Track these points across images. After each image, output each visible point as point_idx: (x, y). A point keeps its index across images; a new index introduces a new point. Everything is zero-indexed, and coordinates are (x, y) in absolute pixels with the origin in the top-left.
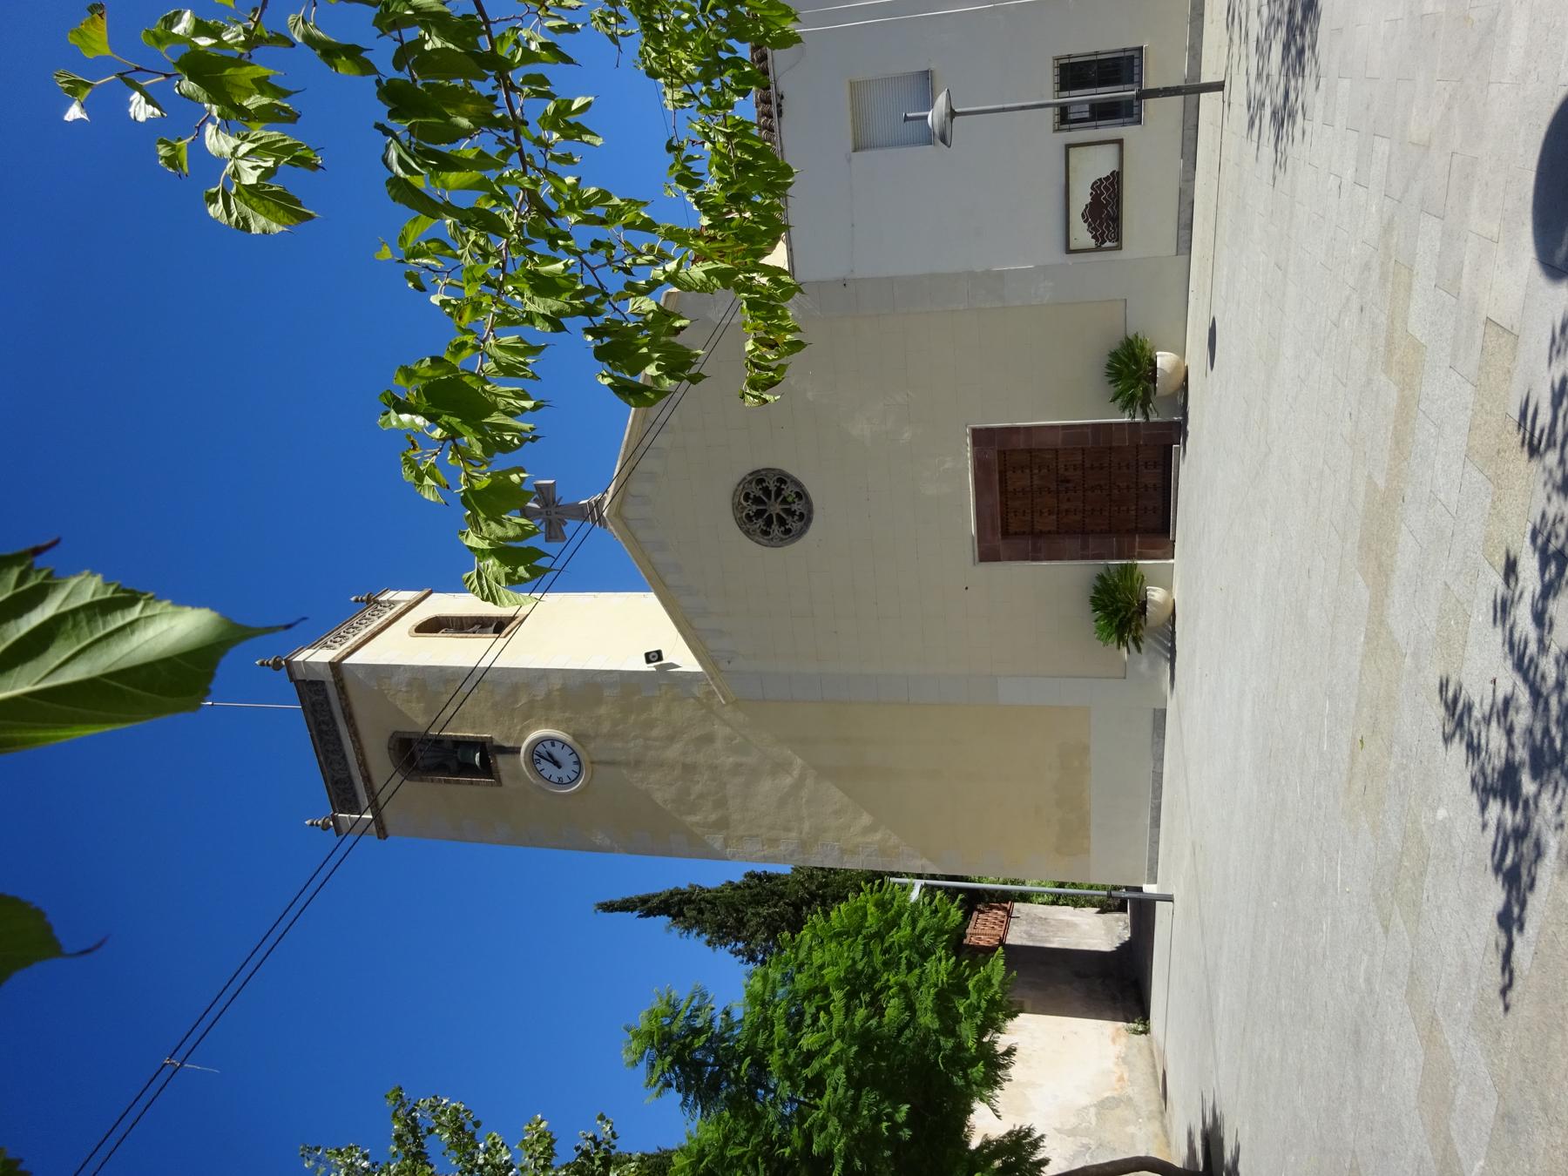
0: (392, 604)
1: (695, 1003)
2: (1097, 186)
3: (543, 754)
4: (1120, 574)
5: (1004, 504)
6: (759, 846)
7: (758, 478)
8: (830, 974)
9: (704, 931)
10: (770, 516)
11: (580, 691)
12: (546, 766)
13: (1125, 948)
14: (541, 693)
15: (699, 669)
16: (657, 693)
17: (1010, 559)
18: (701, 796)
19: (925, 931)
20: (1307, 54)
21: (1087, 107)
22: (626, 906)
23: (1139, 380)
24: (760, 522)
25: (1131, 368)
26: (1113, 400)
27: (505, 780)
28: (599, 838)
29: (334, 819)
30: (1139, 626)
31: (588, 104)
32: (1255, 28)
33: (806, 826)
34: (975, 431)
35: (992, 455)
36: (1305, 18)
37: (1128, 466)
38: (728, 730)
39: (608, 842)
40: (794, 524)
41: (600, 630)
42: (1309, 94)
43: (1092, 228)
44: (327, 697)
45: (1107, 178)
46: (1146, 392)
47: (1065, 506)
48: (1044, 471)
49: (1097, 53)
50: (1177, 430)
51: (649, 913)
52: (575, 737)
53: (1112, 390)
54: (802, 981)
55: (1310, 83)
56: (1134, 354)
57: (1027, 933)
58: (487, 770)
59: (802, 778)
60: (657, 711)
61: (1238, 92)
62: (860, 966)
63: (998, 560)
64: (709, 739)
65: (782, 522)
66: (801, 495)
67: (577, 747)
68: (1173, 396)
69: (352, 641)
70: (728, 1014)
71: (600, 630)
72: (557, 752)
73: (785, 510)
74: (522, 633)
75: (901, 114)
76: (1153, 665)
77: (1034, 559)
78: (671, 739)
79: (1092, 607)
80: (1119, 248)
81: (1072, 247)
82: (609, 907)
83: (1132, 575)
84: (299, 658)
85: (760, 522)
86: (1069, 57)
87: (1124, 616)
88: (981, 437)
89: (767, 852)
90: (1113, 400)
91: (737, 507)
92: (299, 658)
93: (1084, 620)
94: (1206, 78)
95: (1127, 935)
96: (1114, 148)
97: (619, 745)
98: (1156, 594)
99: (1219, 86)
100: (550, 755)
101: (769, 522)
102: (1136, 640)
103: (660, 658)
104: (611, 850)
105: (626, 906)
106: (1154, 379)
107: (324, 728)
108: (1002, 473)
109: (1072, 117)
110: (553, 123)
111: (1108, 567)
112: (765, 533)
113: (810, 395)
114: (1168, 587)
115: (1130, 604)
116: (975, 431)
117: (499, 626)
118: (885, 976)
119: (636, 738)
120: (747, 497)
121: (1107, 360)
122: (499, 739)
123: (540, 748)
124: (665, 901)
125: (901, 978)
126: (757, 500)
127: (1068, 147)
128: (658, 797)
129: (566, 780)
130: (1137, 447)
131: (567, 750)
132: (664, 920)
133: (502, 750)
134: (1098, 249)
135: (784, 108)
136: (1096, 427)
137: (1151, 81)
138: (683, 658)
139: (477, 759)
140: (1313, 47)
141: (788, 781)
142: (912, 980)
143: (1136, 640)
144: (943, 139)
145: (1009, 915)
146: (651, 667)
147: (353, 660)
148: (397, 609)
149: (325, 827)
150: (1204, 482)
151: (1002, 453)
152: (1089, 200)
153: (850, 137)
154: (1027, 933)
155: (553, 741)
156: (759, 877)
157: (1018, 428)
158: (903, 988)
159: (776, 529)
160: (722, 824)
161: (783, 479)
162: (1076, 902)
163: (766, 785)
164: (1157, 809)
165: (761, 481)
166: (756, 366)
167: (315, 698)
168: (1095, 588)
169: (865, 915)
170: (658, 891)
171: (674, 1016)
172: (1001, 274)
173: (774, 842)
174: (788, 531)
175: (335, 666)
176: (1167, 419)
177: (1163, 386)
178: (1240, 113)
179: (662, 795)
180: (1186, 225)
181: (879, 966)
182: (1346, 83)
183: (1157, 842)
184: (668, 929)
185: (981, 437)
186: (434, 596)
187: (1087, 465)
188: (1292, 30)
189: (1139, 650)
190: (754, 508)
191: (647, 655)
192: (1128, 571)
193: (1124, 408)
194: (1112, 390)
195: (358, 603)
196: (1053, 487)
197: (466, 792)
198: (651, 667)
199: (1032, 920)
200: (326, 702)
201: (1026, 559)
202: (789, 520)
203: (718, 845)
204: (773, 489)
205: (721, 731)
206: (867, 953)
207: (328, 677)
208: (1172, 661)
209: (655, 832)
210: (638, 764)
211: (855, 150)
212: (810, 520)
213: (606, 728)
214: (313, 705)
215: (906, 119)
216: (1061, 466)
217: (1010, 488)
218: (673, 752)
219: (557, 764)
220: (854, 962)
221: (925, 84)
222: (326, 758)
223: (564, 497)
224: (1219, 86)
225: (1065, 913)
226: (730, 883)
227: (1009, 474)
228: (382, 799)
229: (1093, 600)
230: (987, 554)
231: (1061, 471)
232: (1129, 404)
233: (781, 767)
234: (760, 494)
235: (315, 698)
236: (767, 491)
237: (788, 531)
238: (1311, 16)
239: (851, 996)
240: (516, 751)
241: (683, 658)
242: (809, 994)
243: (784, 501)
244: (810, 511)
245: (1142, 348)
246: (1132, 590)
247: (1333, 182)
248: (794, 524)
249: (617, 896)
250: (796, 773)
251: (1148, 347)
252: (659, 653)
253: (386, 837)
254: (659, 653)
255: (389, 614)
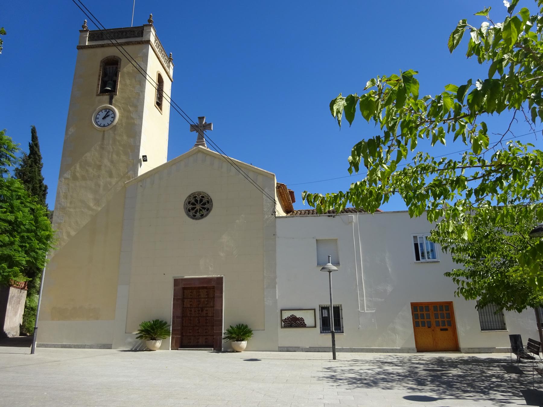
0: (169, 67)
1: (12, 159)
2: (302, 319)
3: (109, 113)
4: (167, 330)
5: (195, 288)
6: (64, 191)
7: (209, 202)
8: (20, 215)
9: (22, 167)
10: (195, 205)
11: (133, 130)
12: (103, 114)
13: (5, 335)
14: (134, 115)
15: (139, 175)
16: (131, 158)
17: (174, 290)
18: (87, 171)
19: (37, 253)
20: (355, 385)
21: (326, 315)
22: (34, 137)
23: (238, 335)
24: (193, 201)
25: (241, 332)
26: (231, 327)
27: (99, 98)
28: (72, 130)
29: (87, 31)
30: (146, 337)
31: (444, 144)
32: (356, 368)
33: (72, 210)
34: (222, 278)
35: (213, 284)
36: (365, 384)
37: (206, 332)
38: (114, 183)
39: (70, 133)
40: (192, 213)
41: (155, 141)
42: (344, 387)
43: (288, 318)
44: (136, 37)
45: (304, 323)
46: (233, 338)
47: (193, 310)
48: (206, 303)
49: (342, 318)
50: (218, 349)
51: (31, 147)
52: (115, 126)
53: (234, 326)
54: (17, 203)
55: (347, 387)
56: (246, 333)
57: (14, 295)
58: (103, 91)
59: (92, 210)
60: (124, 158)
61: (334, 364)
62: (22, 227)
63: (175, 286)
64: (111, 176)
65: (193, 209)
66: (202, 216)
67: (110, 126)
68: (231, 347)
69: (157, 50)
70: (6, 171)
71: (155, 141)
72: (109, 119)
73: (197, 210)
74: (156, 110)
75: (326, 257)
76: (130, 343)
77: (174, 299)
78: (112, 162)
79: (154, 320)
80: (282, 327)
81: (283, 312)
82: (33, 131)
83: (167, 335)
84: (152, 30)
85: (193, 201)
86: (342, 310)
87: (151, 332)
88: (219, 280)
89: (62, 194)
90: (231, 327)
91: (199, 193)
92: (152, 30)
93: (150, 317)
94: (337, 354)
95: (10, 336)
96: (314, 325)
97: (111, 142)
98: (158, 344)
99: (334, 358)
100: (108, 116)
101: (193, 204)
102: (141, 337)
103: (144, 161)
104: (67, 133)
105: (34, 137)
106: (238, 341)
107: (124, 34)
108: (206, 288)
109: (323, 311)
110: (441, 132)
111: (169, 326)
112: (189, 203)
113: (237, 221)
114: (161, 348)
115: (156, 334)
116: (222, 278)
117: (159, 104)
118: (18, 237)
119: (113, 148)
120: (203, 197)
121: (245, 324)
122: (116, 98)
123: (111, 112)
124: (36, 153)
125: (16, 243)
126: (201, 201)
127: (315, 310)
128: (88, 154)
129: (97, 120)
130: (213, 336)
131: (110, 122)
132: (28, 152)
133: (111, 98)
134: (282, 320)
135: (330, 217)
136: (221, 321)
137: (336, 336)
138: (143, 169)
139: (108, 88)
140: (358, 387)
141: (91, 205)
142: (16, 247)
143: (141, 337)
144: (323, 268)
145: (22, 289)
146: (141, 157)
147: (150, 49)
148: (167, 68)
149: (83, 27)
150: (200, 361)
151: (214, 288)
152: (298, 317)
153: (320, 239)
154: (14, 295)
155: (114, 118)
156: (45, 191)
157: (222, 293)
158: (12, 243)
159: (190, 206)
160: (75, 178)
161: (208, 210)
162: (25, 316)
163: (90, 196)
164: (70, 347)
165: (208, 202)
166: (315, 197)
167: (136, 32)
168: (162, 321)
169: (44, 231)
170: (41, 151)
171: (7, 149)
172: (275, 287)
173: (66, 197)
174: (189, 211)
175: (148, 42)
176: (223, 346)
177: (235, 344)
178: (329, 365)
179: (89, 156)
180: (288, 349)
181: (22, 234)
182: (353, 398)
183: (55, 347)
184: (23, 153)
185: (219, 280)
186: (171, 83)
187: (207, 318)
188: (360, 380)
189: (137, 338)
190: (199, 199)
191: (146, 156)
192: (168, 333)
193: (228, 330)
194: (234, 326)
195: (169, 56)
196: (200, 306)
197: (95, 82)
198: (141, 157)
199: (19, 298)
200: (135, 36)
201: (174, 296)
202: (193, 211)
203: (66, 175)
204: (205, 206)
205: (114, 181)
206: (28, 231)
207: (144, 39)
208: (131, 351)
209: (71, 153)
210: (102, 148)
211: (317, 240)
212: (193, 219)
213: (118, 138)
214: (134, 31)
215: (329, 257)
216: (208, 309)
217: (200, 290)
218: (106, 162)
219: (104, 118)
220: (24, 225)
221: (337, 264)
222: (112, 32)
223: (207, 132)
224: (334, 358)
225: (21, 311)
226: (43, 179)
227: (206, 290)
228: (120, 48)
229: (157, 321)
230: (177, 282)
231: (206, 309)
232: (229, 332)
233: (97, 202)
234: (204, 202)
235: (136, 32)
236: (204, 204)
237: (189, 211)
238: (366, 385)
239: (10, 223)
240: (111, 103)
241: (143, 169)
242: (12, 206)
243: (200, 210)
244: (196, 219)
245: (248, 336)
246: (161, 334)
247: (321, 396)
248: (192, 213)
249: (38, 135)
250: (94, 208)
251: (248, 338)
252: (146, 161)
253: (78, 49)
254: (146, 161)
255: (165, 65)
